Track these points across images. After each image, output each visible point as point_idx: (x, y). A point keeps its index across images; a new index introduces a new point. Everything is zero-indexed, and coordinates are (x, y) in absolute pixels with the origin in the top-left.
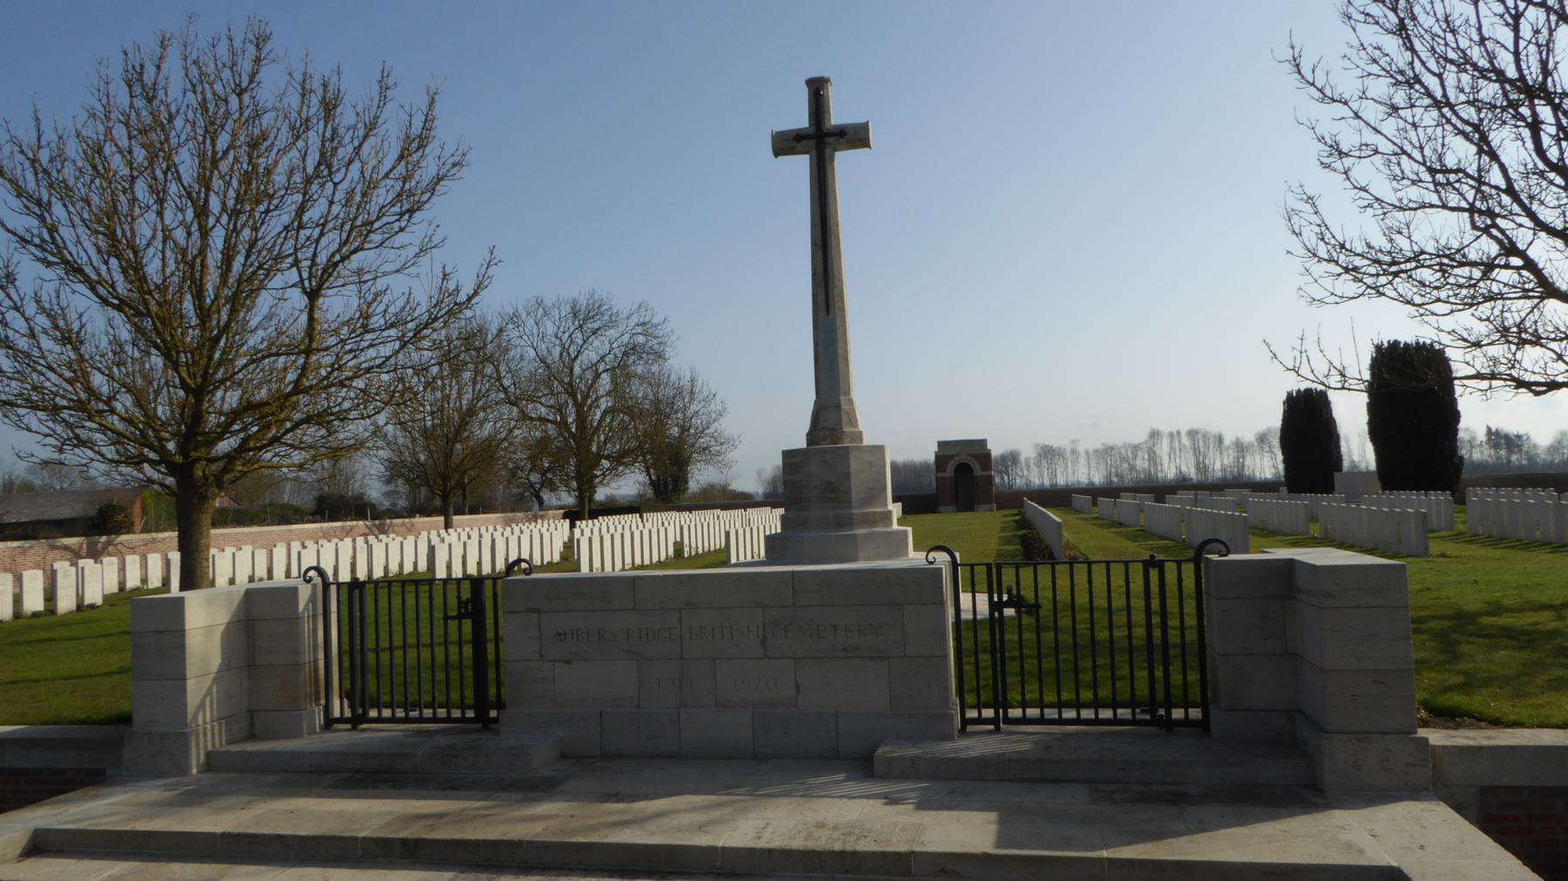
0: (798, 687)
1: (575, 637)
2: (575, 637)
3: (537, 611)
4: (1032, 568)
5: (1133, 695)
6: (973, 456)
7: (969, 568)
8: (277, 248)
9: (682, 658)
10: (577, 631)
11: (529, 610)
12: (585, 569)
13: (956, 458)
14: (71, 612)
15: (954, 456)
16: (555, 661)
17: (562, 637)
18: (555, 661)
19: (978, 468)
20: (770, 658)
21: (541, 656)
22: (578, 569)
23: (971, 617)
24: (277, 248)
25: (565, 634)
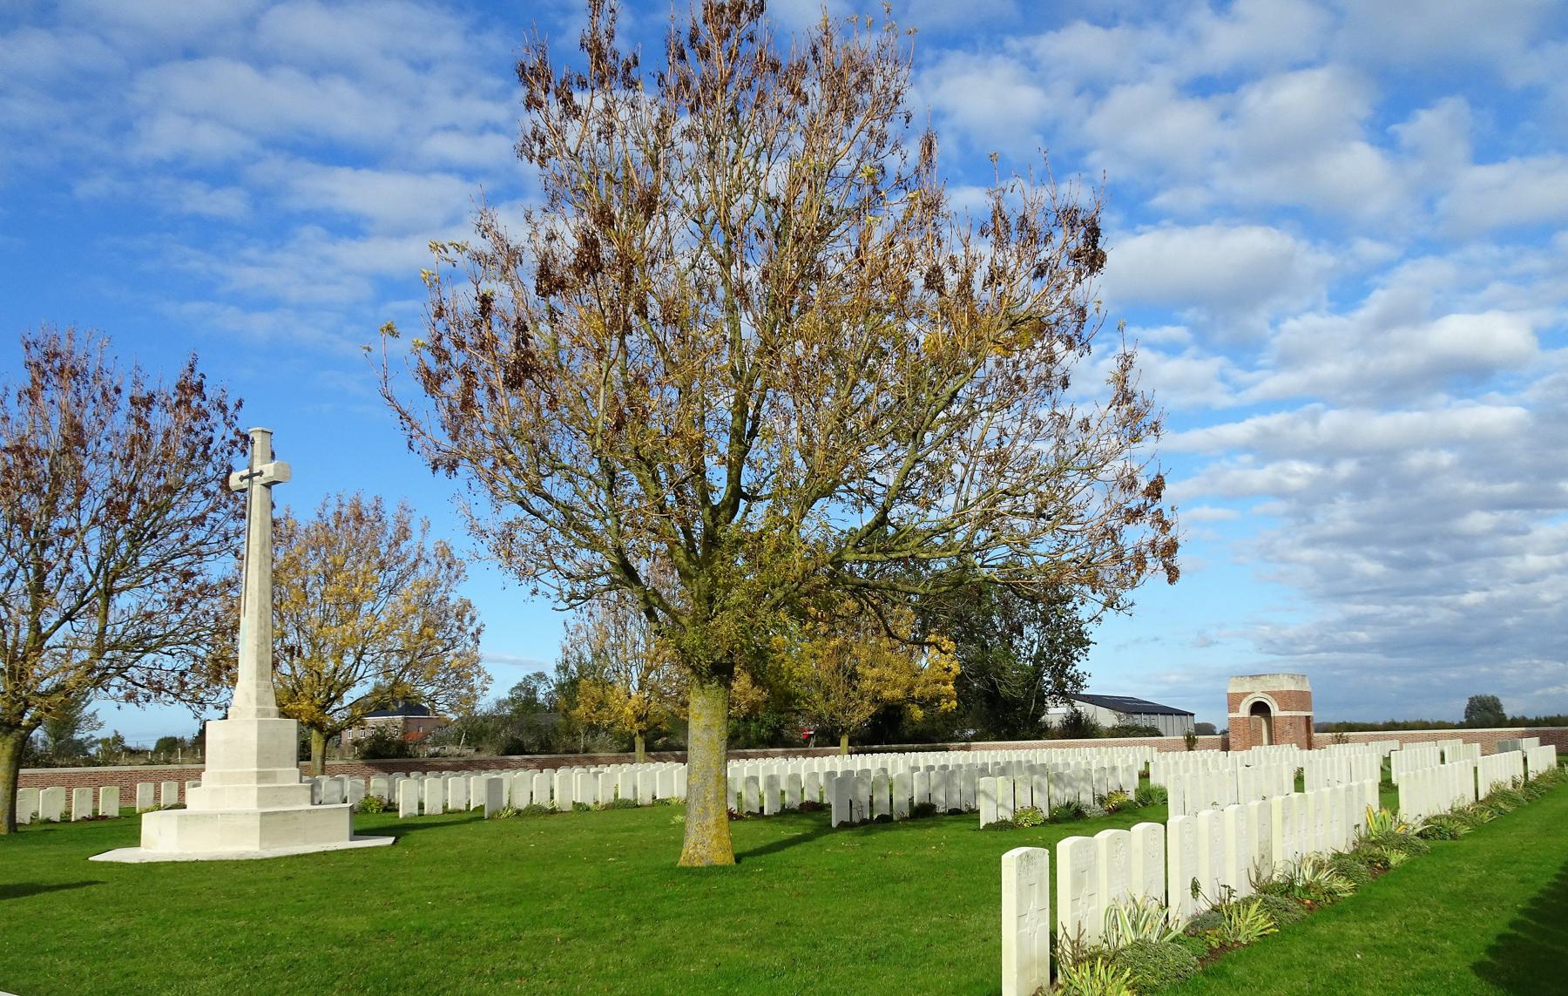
6: (1272, 694)
13: (1250, 696)
15: (1245, 694)
19: (1277, 708)
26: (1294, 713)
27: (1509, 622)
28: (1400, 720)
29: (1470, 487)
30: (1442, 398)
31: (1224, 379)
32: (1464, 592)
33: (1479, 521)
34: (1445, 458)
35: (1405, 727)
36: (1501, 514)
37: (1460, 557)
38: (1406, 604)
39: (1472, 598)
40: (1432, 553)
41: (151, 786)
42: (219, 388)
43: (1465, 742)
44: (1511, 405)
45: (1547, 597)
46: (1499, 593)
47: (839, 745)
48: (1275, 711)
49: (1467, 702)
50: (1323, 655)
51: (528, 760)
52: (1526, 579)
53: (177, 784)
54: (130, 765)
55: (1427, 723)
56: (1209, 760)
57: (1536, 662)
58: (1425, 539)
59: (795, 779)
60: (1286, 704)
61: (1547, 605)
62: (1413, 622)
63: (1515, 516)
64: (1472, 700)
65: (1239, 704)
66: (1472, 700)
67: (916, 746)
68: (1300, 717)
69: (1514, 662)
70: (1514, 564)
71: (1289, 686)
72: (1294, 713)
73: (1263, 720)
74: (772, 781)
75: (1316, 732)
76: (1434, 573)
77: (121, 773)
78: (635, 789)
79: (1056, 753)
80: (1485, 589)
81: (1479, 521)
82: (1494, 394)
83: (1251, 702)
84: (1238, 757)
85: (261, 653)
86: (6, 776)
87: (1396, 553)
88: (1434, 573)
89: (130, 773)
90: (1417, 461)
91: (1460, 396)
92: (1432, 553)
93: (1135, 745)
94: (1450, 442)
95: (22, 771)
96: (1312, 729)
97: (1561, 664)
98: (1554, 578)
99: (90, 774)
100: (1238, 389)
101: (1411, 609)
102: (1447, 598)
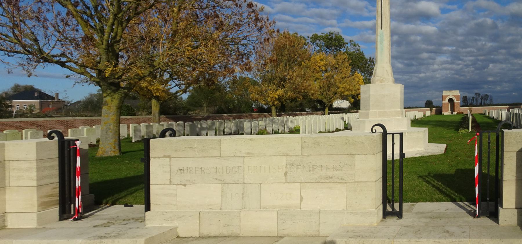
0: (302, 198)
1: (189, 171)
2: (189, 171)
3: (169, 157)
4: (388, 135)
5: (319, 234)
6: (455, 96)
7: (392, 135)
8: (10, 12)
9: (244, 183)
10: (190, 168)
11: (165, 157)
12: (29, 133)
13: (449, 97)
14: (442, 155)
15: (447, 96)
16: (178, 184)
17: (182, 171)
18: (178, 184)
19: (455, 100)
20: (289, 183)
21: (170, 182)
22: (83, 135)
23: (391, 159)
24: (10, 12)
25: (184, 170)
27: (429, 82)
29: (423, 46)
30: (419, 22)
31: (367, 8)
32: (420, 73)
33: (425, 55)
34: (419, 38)
35: (413, 108)
36: (430, 54)
37: (421, 64)
38: (407, 76)
39: (422, 75)
40: (414, 63)
44: (433, 26)
45: (438, 76)
46: (428, 74)
49: (425, 102)
51: (230, 116)
52: (434, 71)
53: (126, 125)
54: (86, 116)
57: (434, 92)
58: (412, 59)
60: (458, 99)
61: (437, 78)
62: (408, 81)
63: (432, 55)
64: (426, 101)
65: (446, 99)
66: (426, 101)
67: (338, 112)
69: (430, 92)
70: (431, 67)
73: (449, 104)
76: (414, 68)
80: (425, 73)
81: (425, 55)
82: (430, 23)
83: (449, 98)
84: (321, 119)
85: (372, 65)
86: (115, 118)
87: (406, 62)
88: (414, 68)
89: (43, 122)
90: (412, 38)
91: (423, 22)
92: (414, 63)
93: (411, 111)
94: (420, 34)
95: (121, 117)
97: (439, 93)
98: (439, 71)
99: (17, 122)
100: (370, 11)
101: (408, 77)
102: (416, 75)
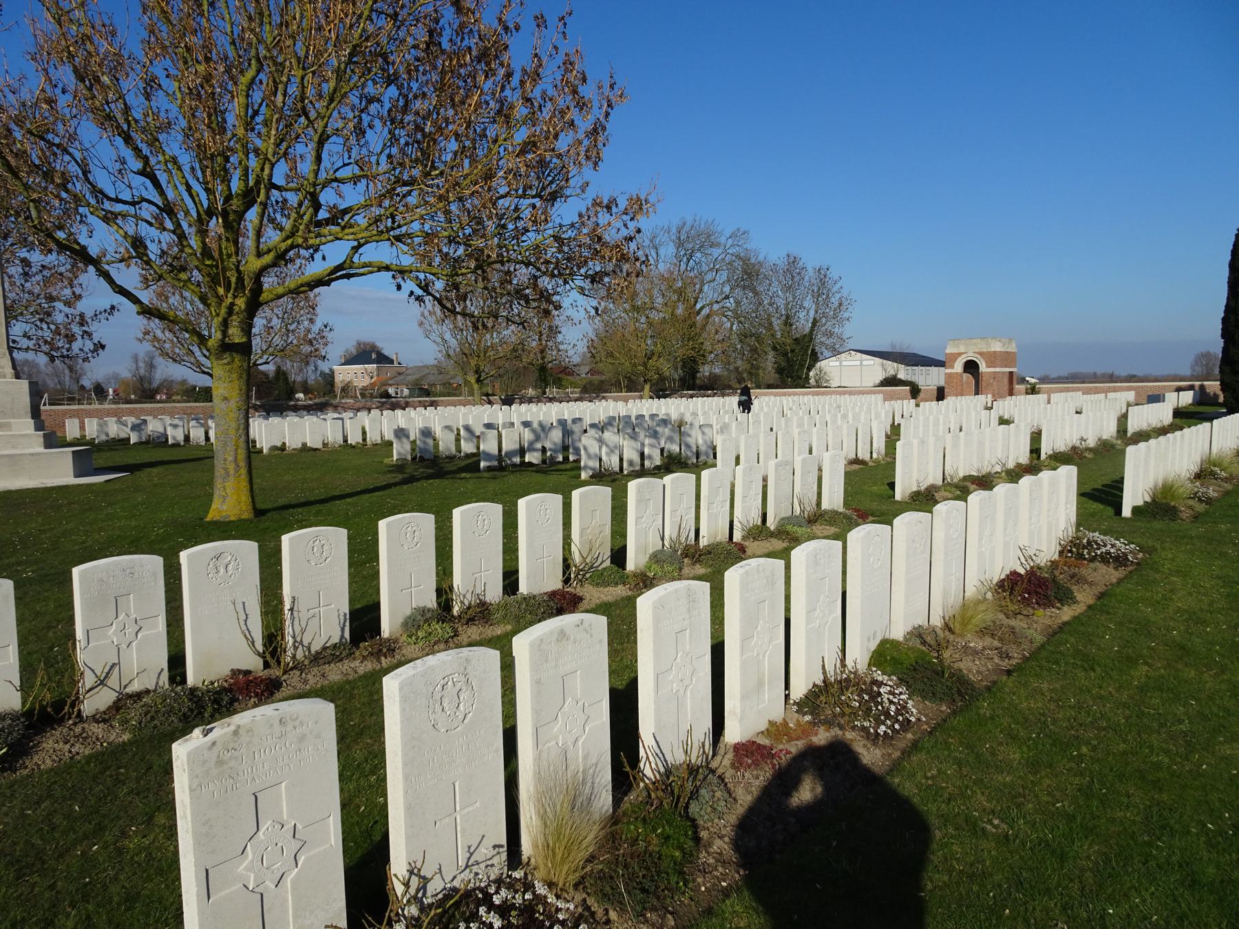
6: (981, 354)
15: (960, 354)
19: (984, 365)
26: (998, 370)
28: (1140, 374)
41: (76, 421)
42: (37, 74)
43: (1083, 394)
47: (211, 401)
48: (983, 368)
50: (291, 641)
55: (1134, 376)
56: (931, 417)
59: (426, 433)
68: (1003, 373)
71: (997, 347)
72: (998, 370)
74: (401, 433)
75: (1018, 384)
77: (70, 410)
78: (364, 433)
79: (788, 401)
96: (1015, 381)
